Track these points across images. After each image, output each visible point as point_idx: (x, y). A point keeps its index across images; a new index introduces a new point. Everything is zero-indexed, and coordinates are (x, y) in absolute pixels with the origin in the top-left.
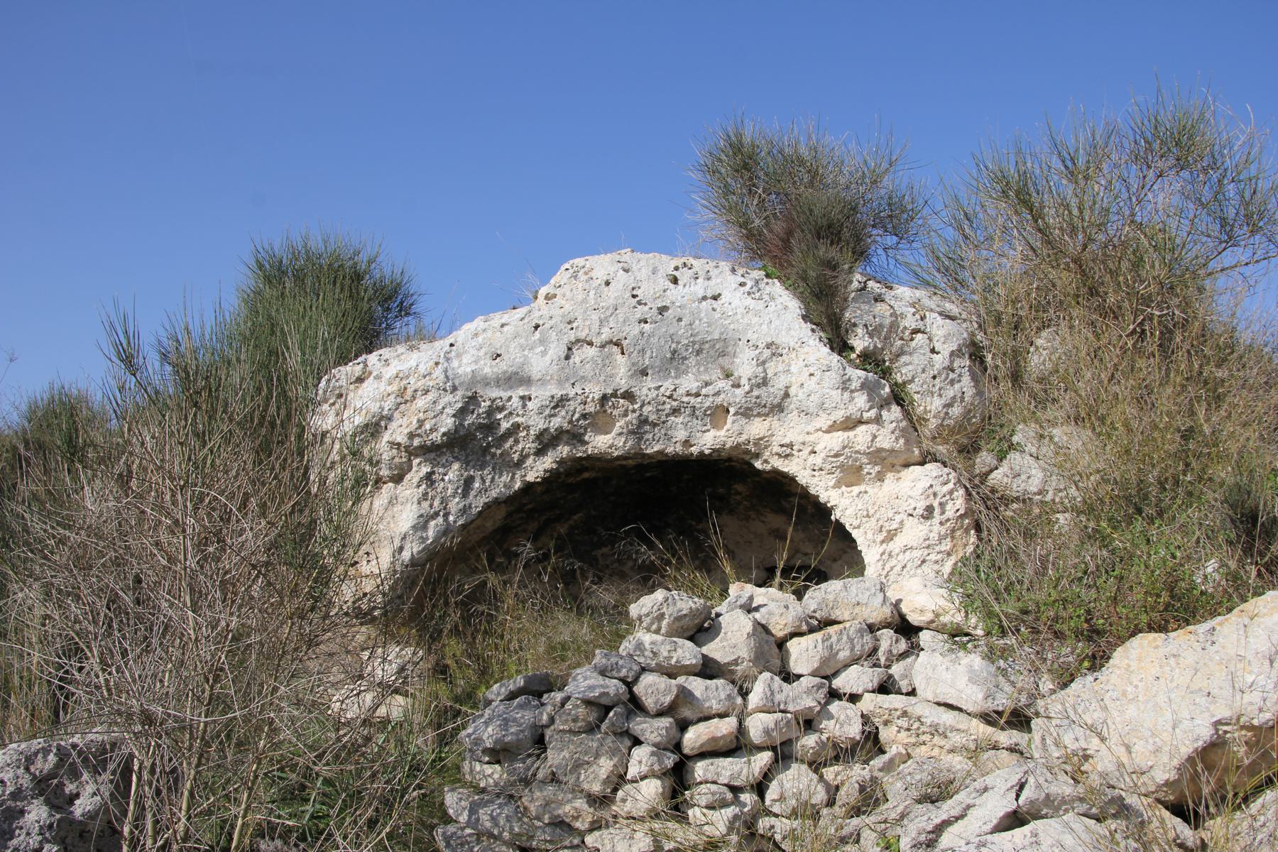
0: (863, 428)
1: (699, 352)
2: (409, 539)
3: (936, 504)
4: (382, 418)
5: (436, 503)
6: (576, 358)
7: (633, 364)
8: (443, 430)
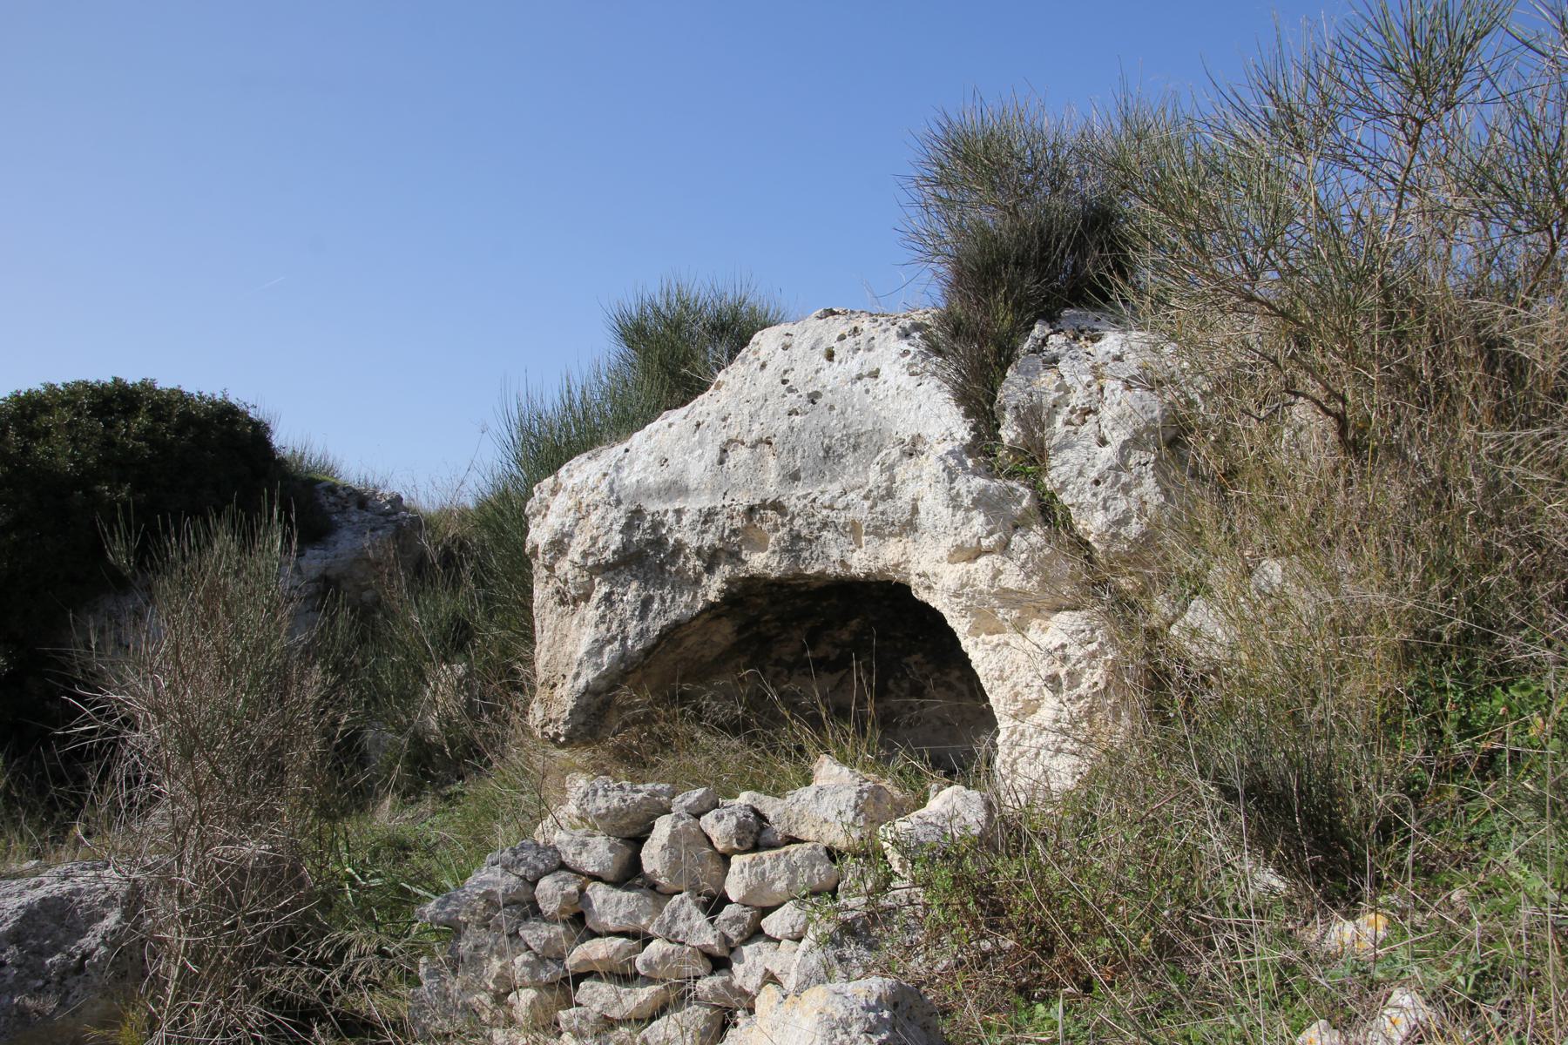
0: (983, 560)
1: (855, 448)
2: (585, 665)
3: (1062, 673)
4: (564, 535)
5: (614, 627)
6: (730, 463)
7: (783, 467)
8: (613, 547)
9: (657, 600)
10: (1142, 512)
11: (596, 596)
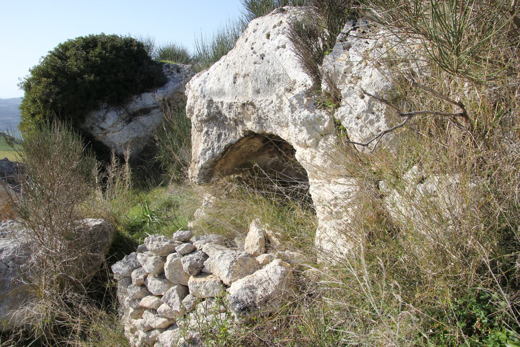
1: (279, 80)
4: (191, 107)
6: (237, 84)
7: (253, 87)
8: (205, 114)
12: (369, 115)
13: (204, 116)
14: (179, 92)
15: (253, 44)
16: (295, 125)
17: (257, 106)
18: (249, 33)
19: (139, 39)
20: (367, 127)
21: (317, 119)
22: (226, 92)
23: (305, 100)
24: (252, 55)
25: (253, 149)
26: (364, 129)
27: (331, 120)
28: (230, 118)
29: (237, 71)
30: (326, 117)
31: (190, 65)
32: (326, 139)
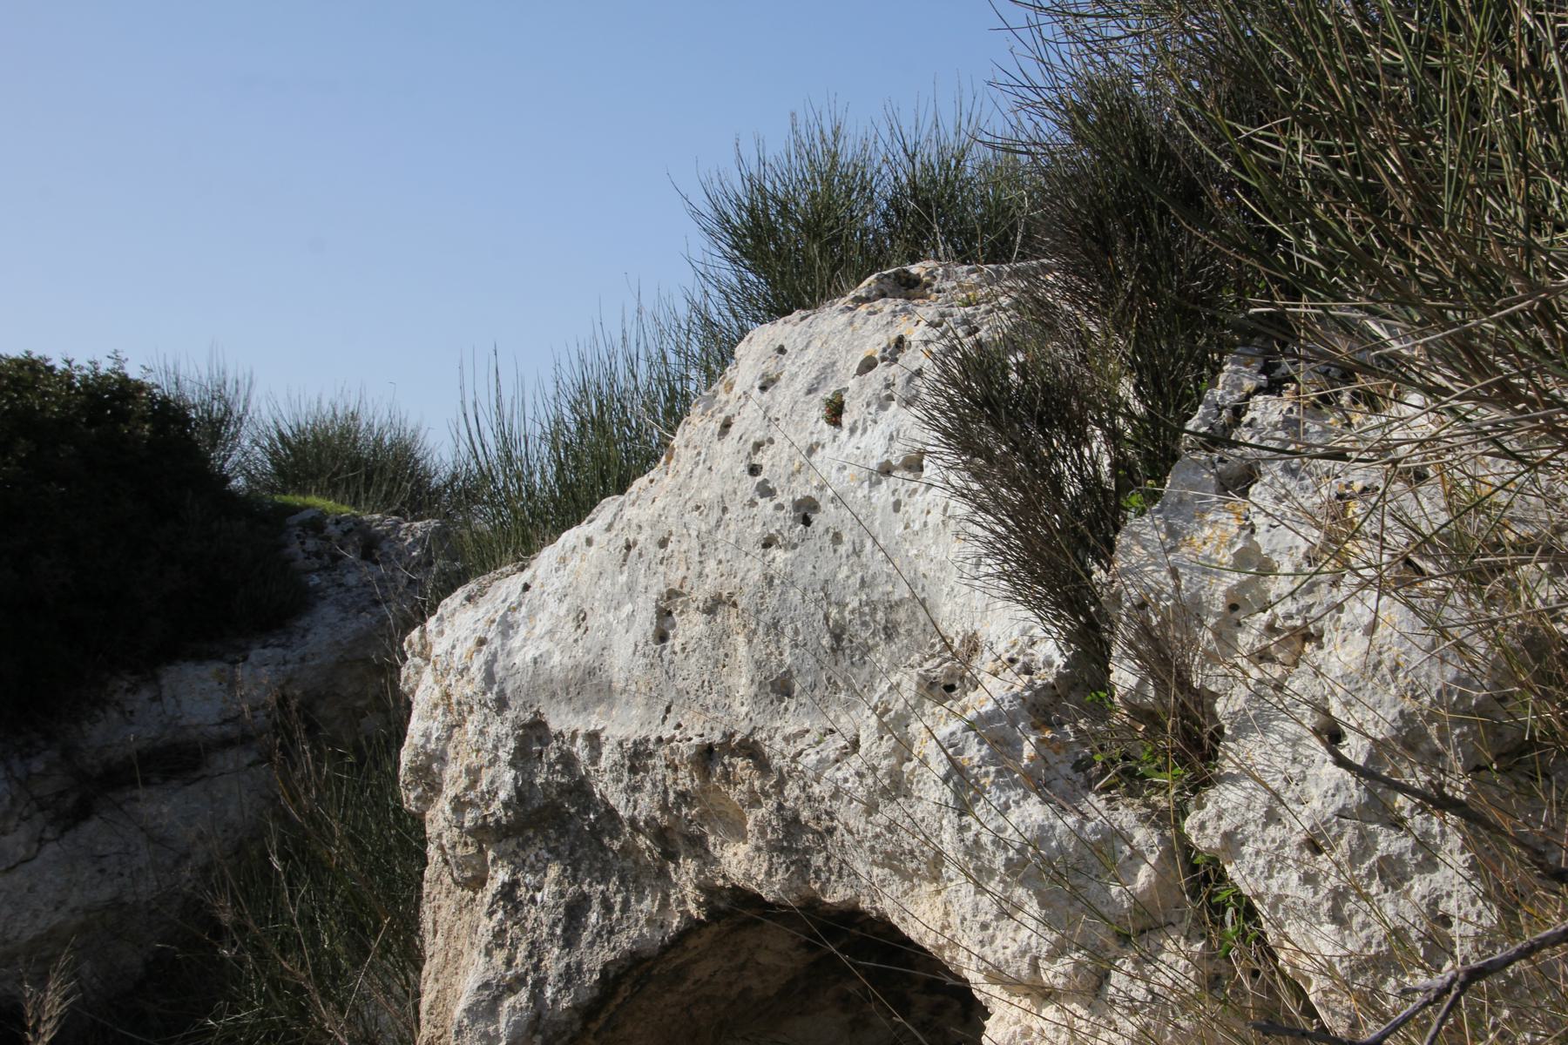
1: (890, 632)
4: (431, 757)
6: (675, 642)
7: (759, 665)
8: (503, 795)
9: (596, 904)
10: (1438, 947)
11: (493, 887)
12: (1373, 835)
13: (496, 806)
14: (367, 661)
15: (758, 446)
16: (979, 878)
17: (776, 762)
18: (737, 390)
19: (164, 386)
20: (1366, 897)
21: (1096, 849)
22: (619, 685)
23: (1028, 750)
24: (753, 503)
25: (755, 983)
26: (1348, 908)
27: (1168, 855)
28: (633, 821)
29: (675, 577)
30: (1140, 835)
31: (434, 523)
32: (1147, 959)
